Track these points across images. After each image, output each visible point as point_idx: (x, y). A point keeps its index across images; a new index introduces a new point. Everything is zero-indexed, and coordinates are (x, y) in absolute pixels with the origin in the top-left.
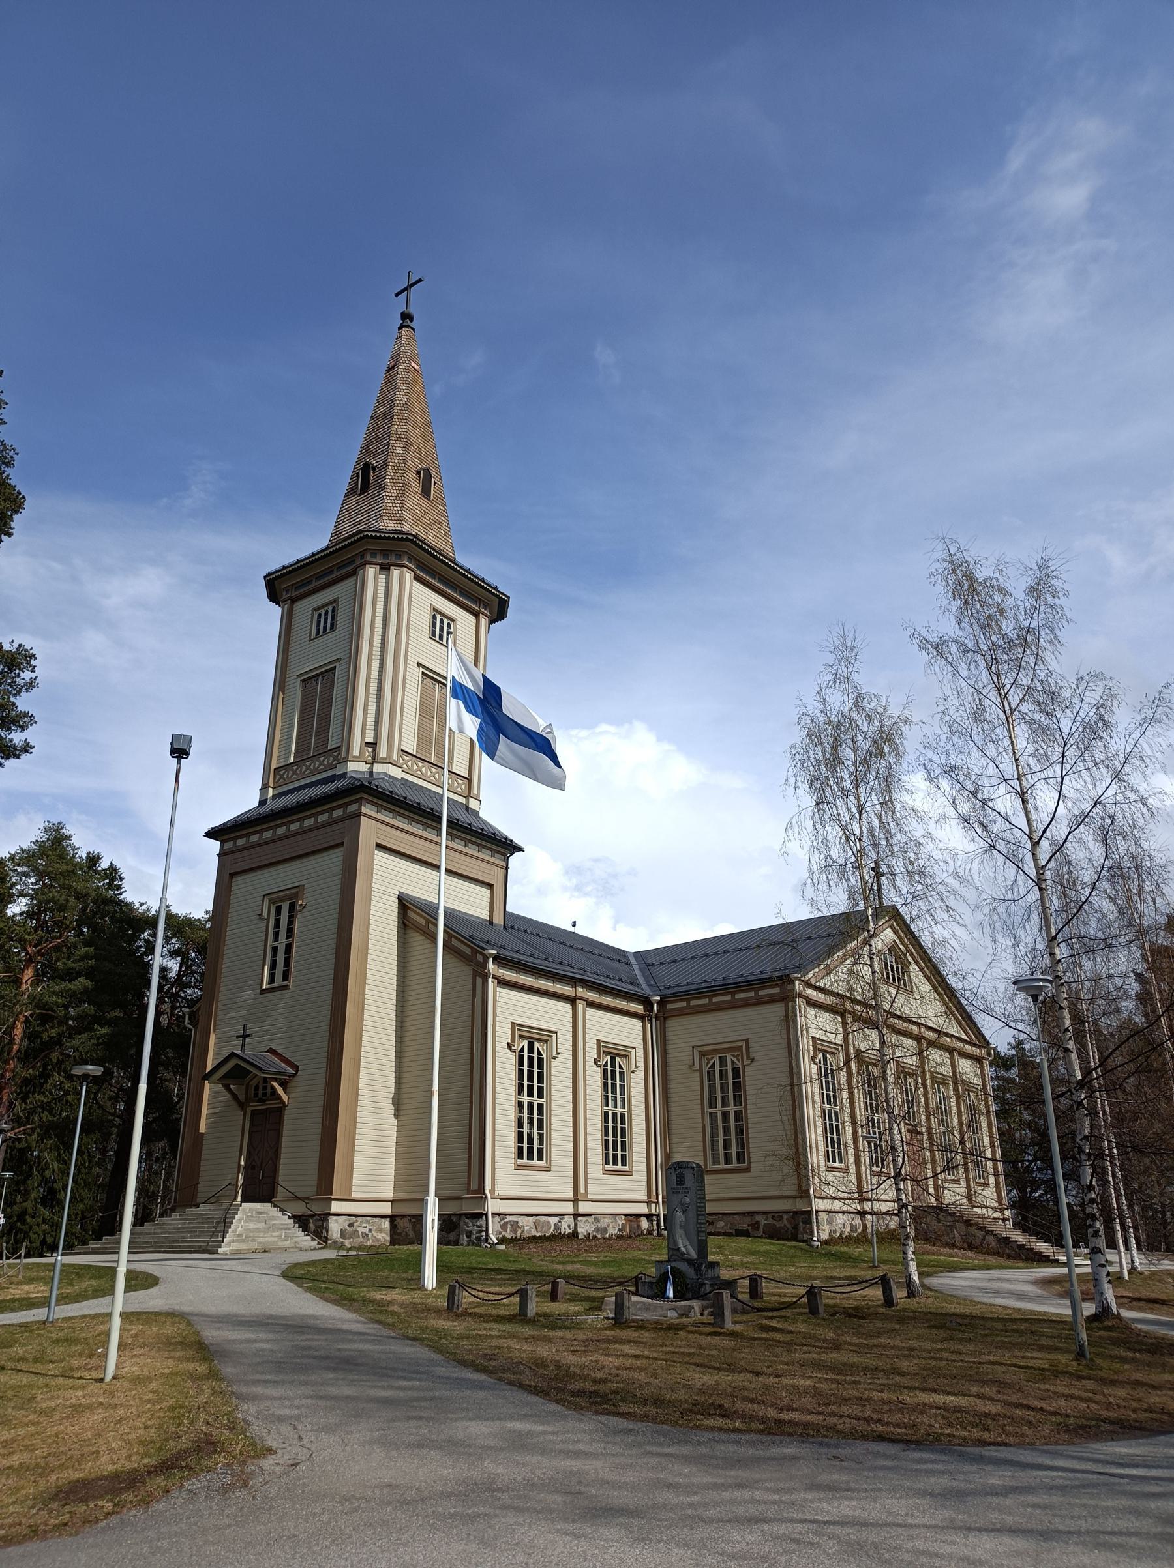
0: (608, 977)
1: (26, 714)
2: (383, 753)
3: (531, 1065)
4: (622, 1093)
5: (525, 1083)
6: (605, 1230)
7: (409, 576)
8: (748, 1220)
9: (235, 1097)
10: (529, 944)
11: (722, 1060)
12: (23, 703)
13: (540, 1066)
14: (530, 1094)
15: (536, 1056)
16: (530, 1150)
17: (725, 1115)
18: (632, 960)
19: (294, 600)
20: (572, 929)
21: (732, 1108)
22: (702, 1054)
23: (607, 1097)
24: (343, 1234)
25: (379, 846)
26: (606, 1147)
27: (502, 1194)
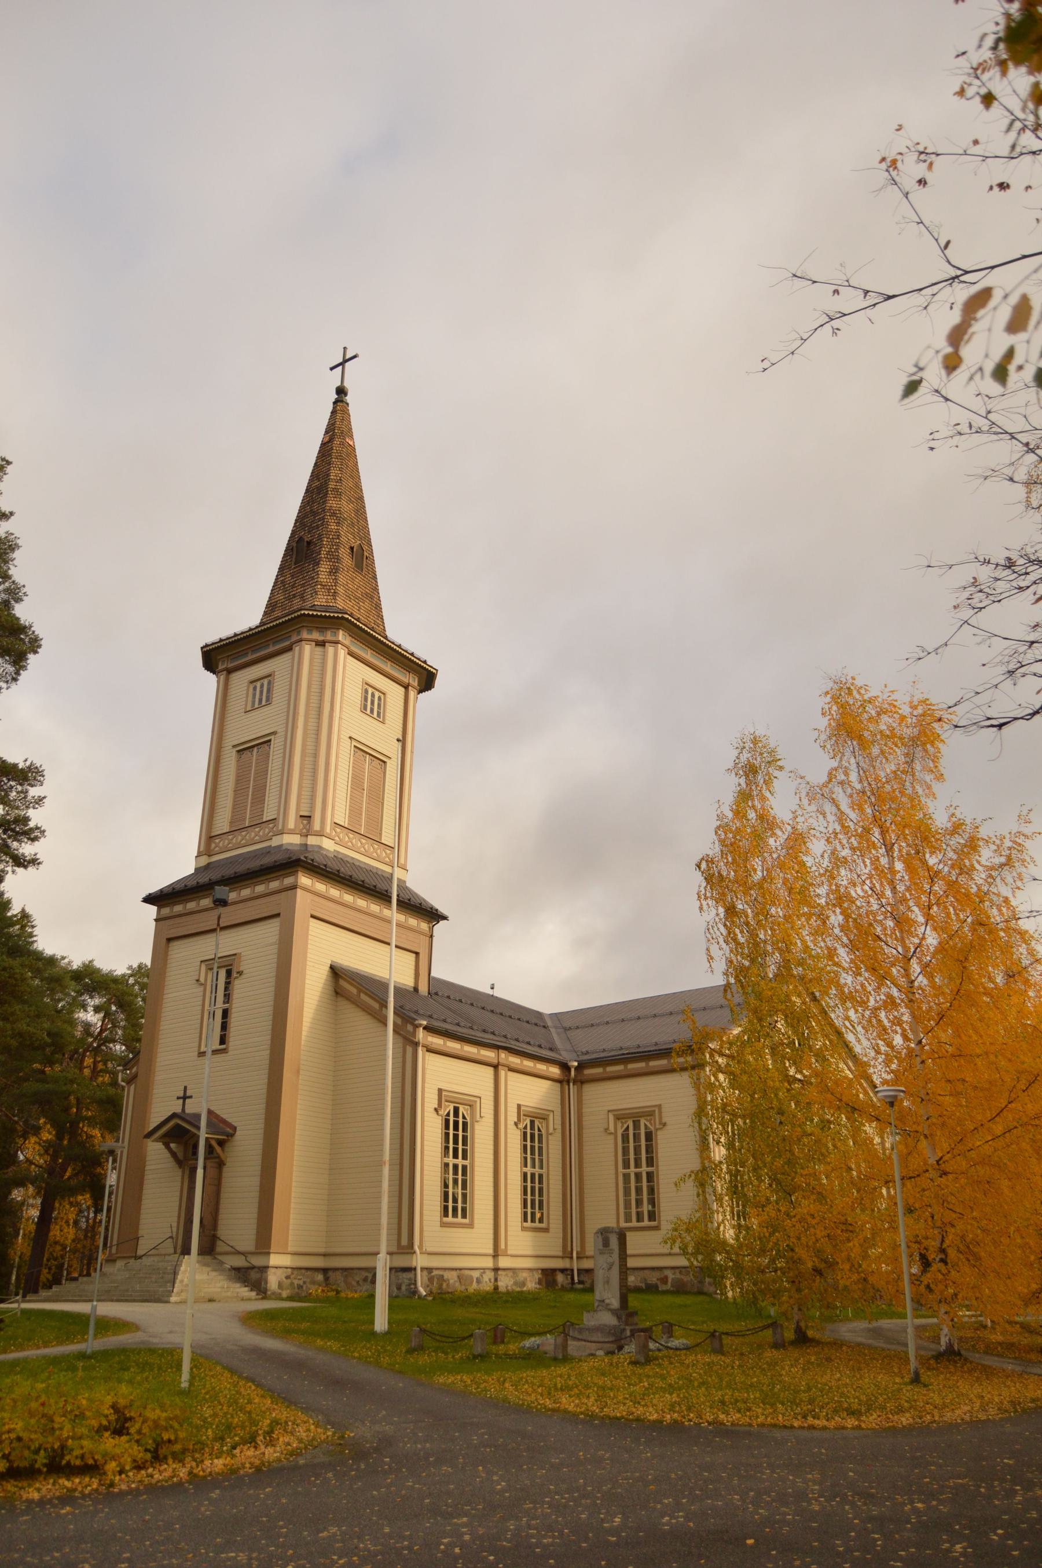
0: (529, 1043)
1: (37, 828)
2: (317, 826)
3: (456, 1128)
4: (540, 1154)
5: (451, 1145)
6: (524, 1284)
7: (342, 652)
9: (174, 1154)
10: (454, 1012)
11: (456, 1110)
12: (36, 817)
13: (465, 1130)
14: (456, 1156)
15: (461, 1120)
16: (455, 1209)
17: (638, 1176)
18: (549, 1023)
19: (230, 671)
20: (490, 992)
21: (644, 1169)
22: (618, 1118)
23: (526, 1158)
24: (280, 1285)
25: (312, 916)
26: (525, 1206)
27: (429, 1250)
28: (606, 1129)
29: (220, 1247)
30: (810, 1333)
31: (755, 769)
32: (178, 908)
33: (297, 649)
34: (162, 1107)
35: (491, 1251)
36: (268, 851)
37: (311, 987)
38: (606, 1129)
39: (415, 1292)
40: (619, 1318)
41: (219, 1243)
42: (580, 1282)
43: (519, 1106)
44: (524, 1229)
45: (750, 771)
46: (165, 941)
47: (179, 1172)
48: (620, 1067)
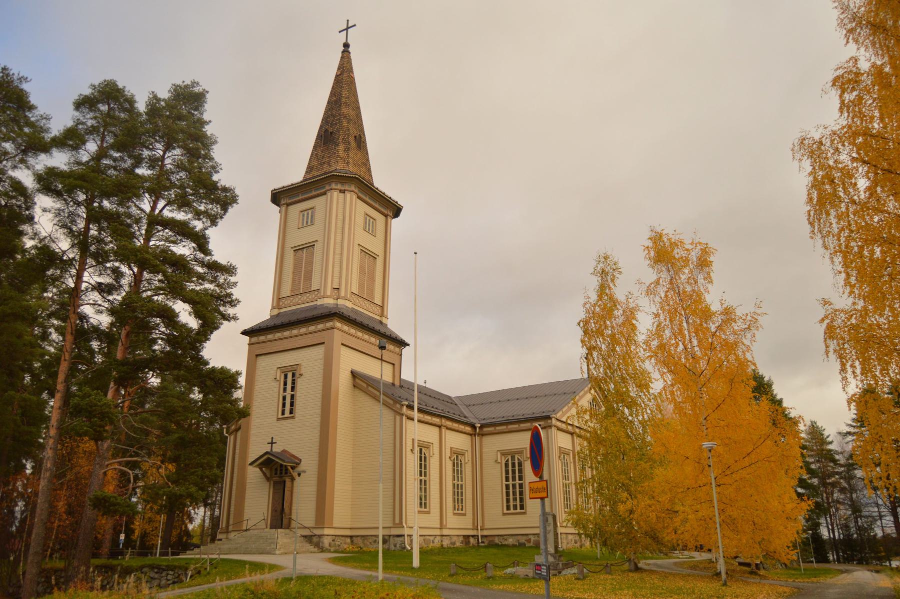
2: (343, 294)
6: (454, 543)
7: (355, 197)
8: (525, 538)
11: (513, 458)
12: (236, 293)
17: (514, 486)
19: (288, 205)
21: (517, 482)
24: (330, 545)
28: (496, 461)
29: (293, 524)
30: (640, 565)
31: (606, 274)
32: (262, 338)
33: (329, 194)
34: (257, 449)
35: (438, 526)
36: (315, 307)
37: (343, 380)
38: (496, 461)
39: (405, 548)
40: (555, 558)
41: (293, 522)
42: (483, 542)
43: (451, 448)
44: (455, 514)
45: (603, 273)
46: (254, 357)
47: (268, 484)
48: (504, 427)
